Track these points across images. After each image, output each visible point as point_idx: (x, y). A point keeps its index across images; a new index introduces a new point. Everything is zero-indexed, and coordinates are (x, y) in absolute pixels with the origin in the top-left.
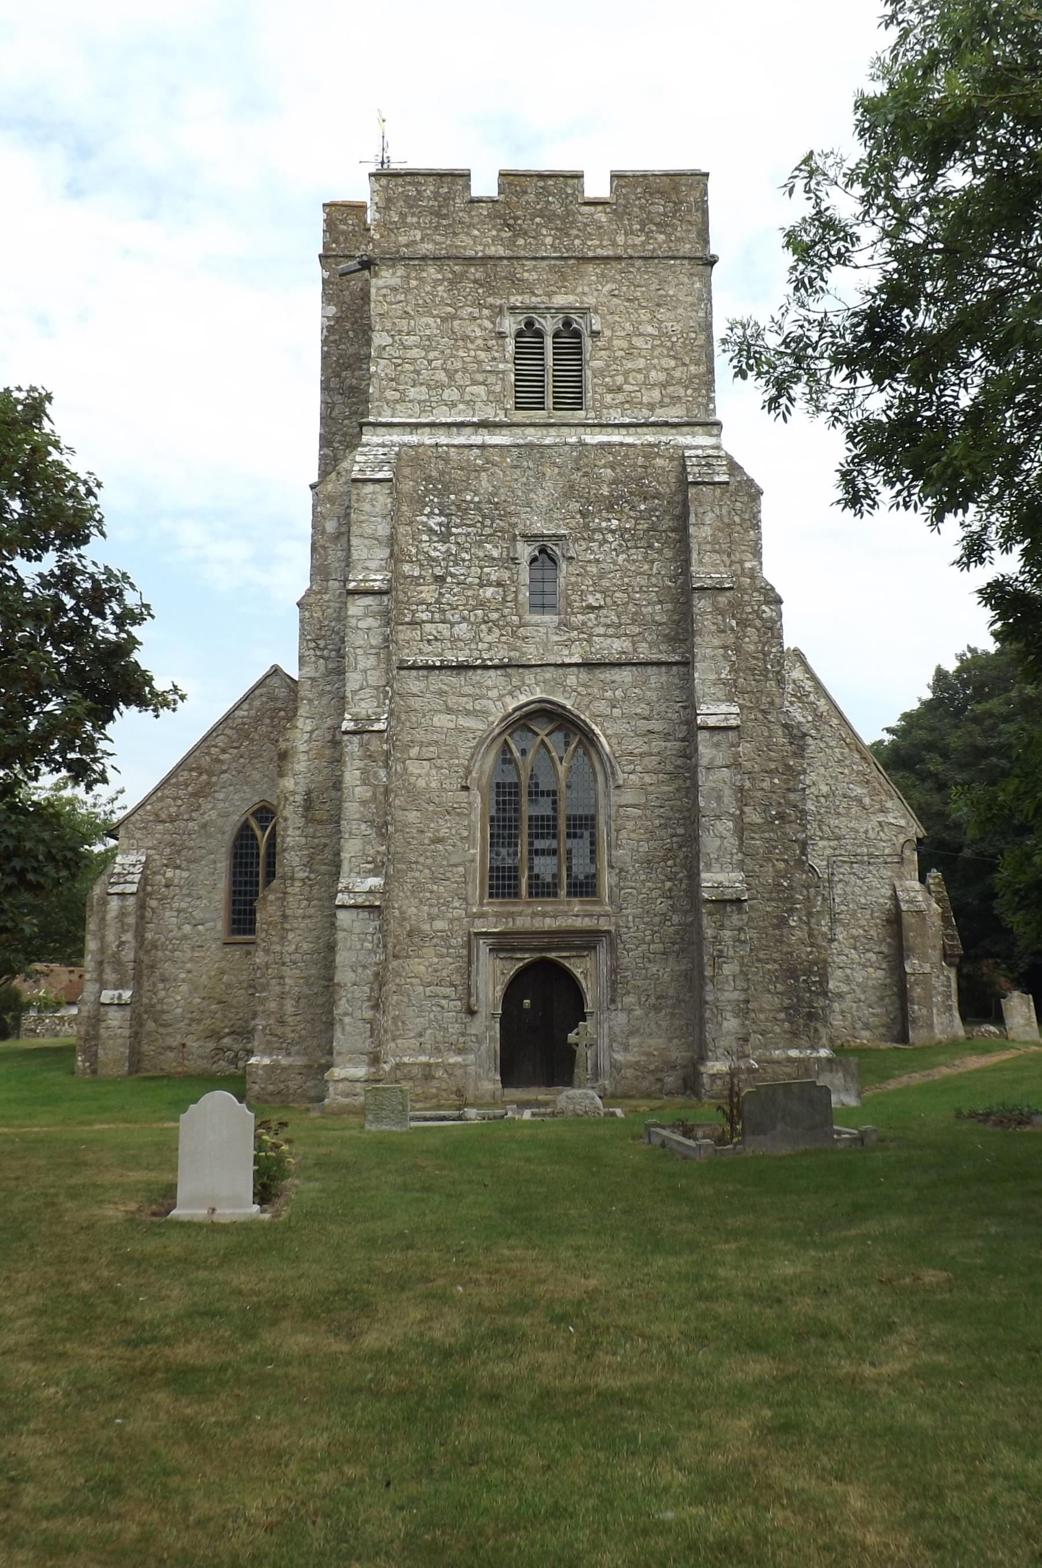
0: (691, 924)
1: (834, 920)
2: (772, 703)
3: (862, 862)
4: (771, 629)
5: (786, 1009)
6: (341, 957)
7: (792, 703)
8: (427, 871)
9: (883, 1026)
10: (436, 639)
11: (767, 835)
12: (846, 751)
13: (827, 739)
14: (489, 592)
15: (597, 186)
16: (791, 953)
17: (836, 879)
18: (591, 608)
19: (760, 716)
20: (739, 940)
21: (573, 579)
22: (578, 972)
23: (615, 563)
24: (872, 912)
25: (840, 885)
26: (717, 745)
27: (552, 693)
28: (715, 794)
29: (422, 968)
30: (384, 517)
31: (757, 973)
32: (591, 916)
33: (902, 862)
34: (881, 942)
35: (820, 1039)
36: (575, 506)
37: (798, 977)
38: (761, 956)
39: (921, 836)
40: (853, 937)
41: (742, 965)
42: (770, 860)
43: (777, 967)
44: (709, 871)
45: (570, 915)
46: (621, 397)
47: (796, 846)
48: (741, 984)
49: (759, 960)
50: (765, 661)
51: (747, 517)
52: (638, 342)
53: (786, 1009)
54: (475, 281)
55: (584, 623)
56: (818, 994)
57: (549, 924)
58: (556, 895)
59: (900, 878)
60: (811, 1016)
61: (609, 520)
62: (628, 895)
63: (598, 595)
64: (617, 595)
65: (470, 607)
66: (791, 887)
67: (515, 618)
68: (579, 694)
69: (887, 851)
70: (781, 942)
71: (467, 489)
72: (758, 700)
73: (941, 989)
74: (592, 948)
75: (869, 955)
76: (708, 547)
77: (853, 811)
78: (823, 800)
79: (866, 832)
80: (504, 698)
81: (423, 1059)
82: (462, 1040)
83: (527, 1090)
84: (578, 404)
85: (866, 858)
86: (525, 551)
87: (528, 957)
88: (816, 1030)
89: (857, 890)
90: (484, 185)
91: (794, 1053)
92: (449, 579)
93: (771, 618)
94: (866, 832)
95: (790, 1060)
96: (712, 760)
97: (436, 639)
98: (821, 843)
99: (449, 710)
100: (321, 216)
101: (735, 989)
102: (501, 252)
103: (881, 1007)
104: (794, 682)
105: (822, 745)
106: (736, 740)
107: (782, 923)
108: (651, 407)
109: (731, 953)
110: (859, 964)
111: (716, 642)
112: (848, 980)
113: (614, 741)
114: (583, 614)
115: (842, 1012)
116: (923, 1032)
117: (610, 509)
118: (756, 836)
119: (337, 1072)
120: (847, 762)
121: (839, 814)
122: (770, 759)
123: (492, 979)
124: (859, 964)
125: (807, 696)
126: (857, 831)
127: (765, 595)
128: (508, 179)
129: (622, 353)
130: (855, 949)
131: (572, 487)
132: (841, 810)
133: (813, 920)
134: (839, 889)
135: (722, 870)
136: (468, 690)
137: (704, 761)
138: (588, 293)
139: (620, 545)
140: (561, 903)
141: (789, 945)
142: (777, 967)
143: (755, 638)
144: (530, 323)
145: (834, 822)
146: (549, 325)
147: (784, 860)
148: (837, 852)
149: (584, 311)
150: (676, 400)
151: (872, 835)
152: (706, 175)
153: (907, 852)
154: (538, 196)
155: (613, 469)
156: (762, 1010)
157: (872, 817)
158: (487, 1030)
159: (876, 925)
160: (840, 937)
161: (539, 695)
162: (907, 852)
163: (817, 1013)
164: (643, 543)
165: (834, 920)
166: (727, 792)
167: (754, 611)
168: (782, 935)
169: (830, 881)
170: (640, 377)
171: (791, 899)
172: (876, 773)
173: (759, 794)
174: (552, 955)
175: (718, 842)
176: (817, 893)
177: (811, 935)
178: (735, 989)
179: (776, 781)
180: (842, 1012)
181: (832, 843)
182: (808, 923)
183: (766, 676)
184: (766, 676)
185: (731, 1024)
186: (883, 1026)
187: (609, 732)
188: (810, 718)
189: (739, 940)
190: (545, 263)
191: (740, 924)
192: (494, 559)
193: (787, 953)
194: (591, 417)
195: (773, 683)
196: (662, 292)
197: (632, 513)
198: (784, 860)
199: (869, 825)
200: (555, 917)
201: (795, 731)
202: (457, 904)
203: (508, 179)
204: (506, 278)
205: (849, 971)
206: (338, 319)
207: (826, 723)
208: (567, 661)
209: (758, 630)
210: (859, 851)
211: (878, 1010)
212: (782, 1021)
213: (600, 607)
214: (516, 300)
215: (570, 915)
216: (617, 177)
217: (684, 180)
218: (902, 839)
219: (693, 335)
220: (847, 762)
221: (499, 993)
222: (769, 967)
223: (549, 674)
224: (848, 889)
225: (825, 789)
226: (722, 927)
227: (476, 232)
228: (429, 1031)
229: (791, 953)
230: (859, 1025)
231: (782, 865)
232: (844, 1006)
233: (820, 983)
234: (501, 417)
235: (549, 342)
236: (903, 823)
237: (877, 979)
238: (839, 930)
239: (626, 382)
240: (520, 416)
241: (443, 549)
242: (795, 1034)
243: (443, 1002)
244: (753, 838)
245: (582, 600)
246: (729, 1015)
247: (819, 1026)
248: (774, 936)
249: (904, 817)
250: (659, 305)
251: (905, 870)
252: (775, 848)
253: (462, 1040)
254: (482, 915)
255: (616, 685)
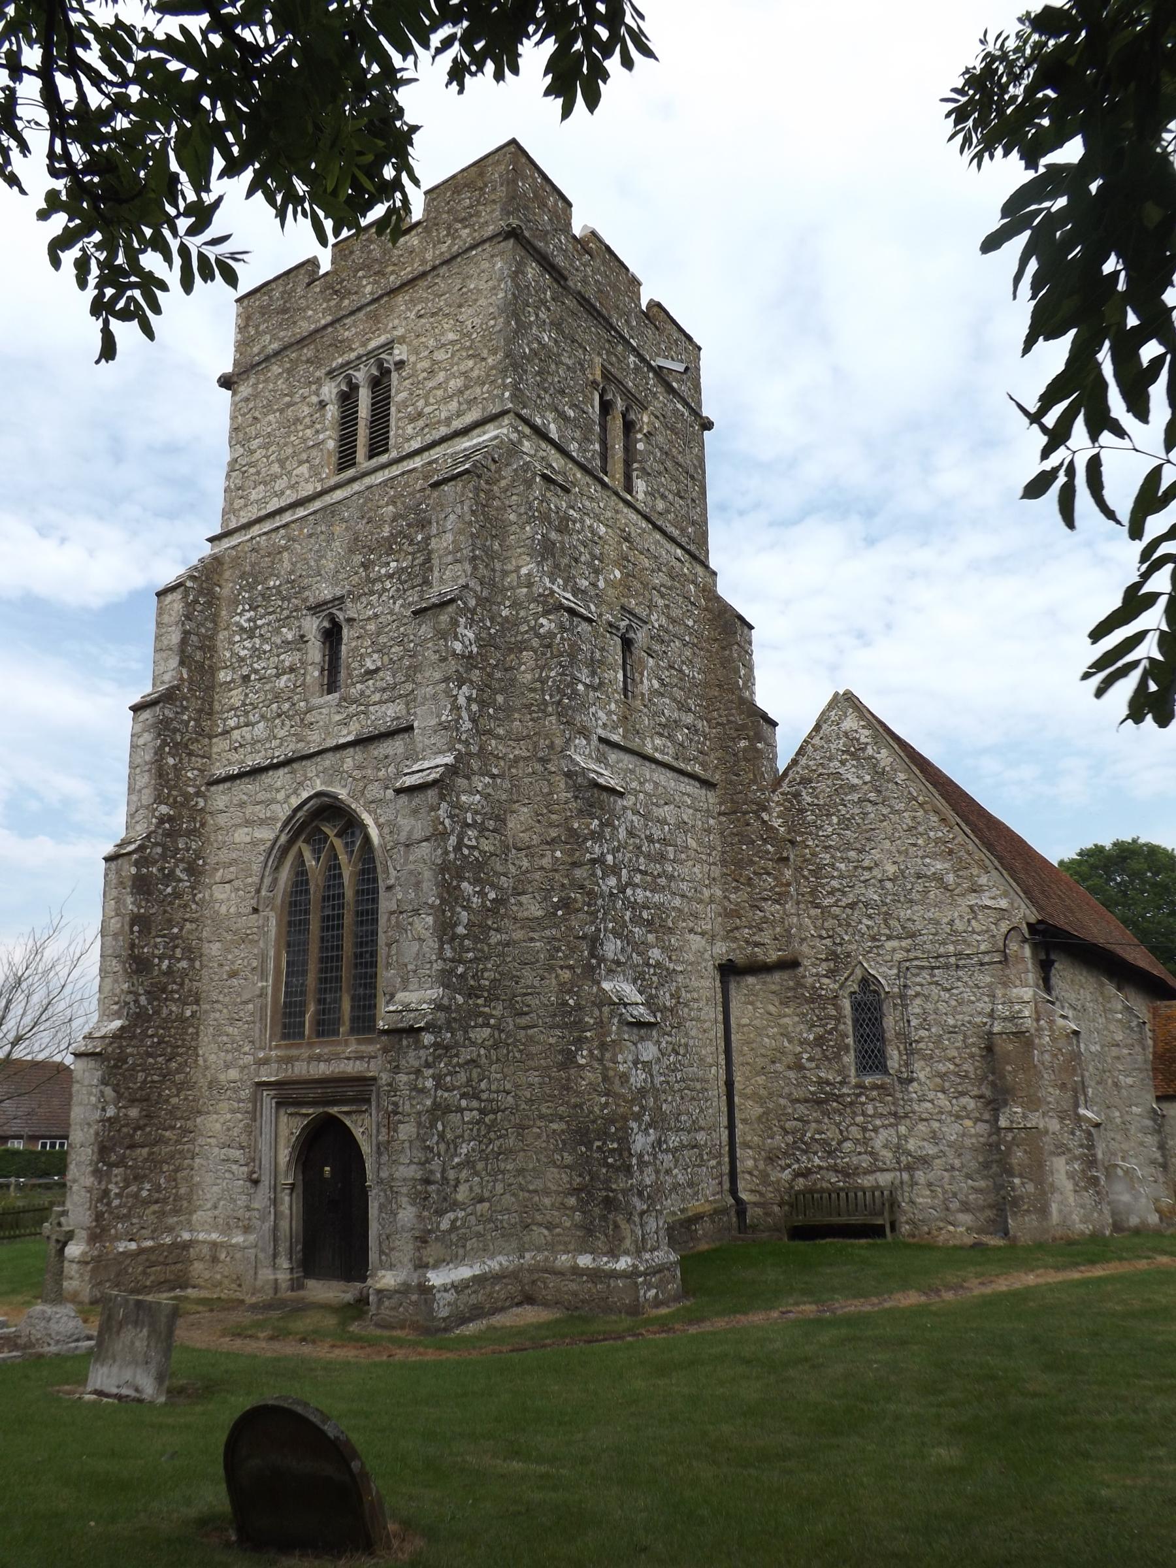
0: (644, 1067)
1: (910, 1050)
2: (551, 746)
3: (947, 967)
4: (549, 646)
5: (575, 1191)
7: (843, 763)
8: (225, 1011)
9: (991, 1207)
10: (241, 746)
11: (548, 933)
12: (920, 813)
13: (893, 802)
14: (282, 682)
16: (580, 1106)
17: (911, 992)
18: (371, 673)
19: (539, 767)
20: (415, 1088)
21: (354, 644)
22: (357, 1132)
23: (391, 613)
24: (965, 1036)
25: (918, 1001)
26: (415, 812)
27: (331, 783)
28: (413, 880)
29: (218, 1126)
30: (177, 624)
31: (539, 1136)
32: (361, 1058)
33: (1005, 961)
34: (982, 1079)
35: (622, 1240)
36: (358, 559)
37: (591, 1143)
38: (544, 1110)
39: (1032, 920)
40: (942, 1076)
41: (419, 1124)
42: (551, 969)
43: (564, 1126)
44: (405, 989)
46: (421, 423)
47: (584, 945)
48: (420, 1155)
49: (542, 1117)
50: (543, 690)
51: (522, 510)
52: (440, 355)
53: (575, 1191)
54: (308, 361)
55: (362, 693)
56: (618, 1170)
57: (322, 1069)
58: (336, 1033)
59: (1005, 985)
60: (609, 1203)
61: (388, 563)
63: (375, 656)
64: (393, 650)
65: (267, 703)
66: (579, 1007)
67: (302, 704)
68: (354, 779)
69: (983, 948)
70: (568, 1089)
71: (272, 575)
72: (535, 745)
73: (1078, 1151)
75: (964, 1100)
76: (450, 558)
77: (932, 895)
78: (889, 885)
79: (951, 923)
80: (286, 795)
81: (214, 1236)
82: (247, 1215)
83: (327, 1283)
85: (952, 960)
86: (312, 626)
88: (617, 1226)
89: (942, 1007)
91: (585, 1261)
92: (253, 677)
93: (549, 632)
94: (951, 923)
95: (576, 1271)
96: (410, 832)
97: (241, 746)
98: (889, 945)
99: (248, 823)
101: (411, 1162)
103: (984, 1178)
104: (846, 734)
105: (885, 811)
106: (435, 800)
107: (569, 1060)
109: (407, 1107)
110: (950, 1113)
111: (438, 676)
112: (934, 1138)
113: (386, 830)
114: (362, 682)
115: (930, 1185)
116: (1032, 1221)
117: (390, 552)
118: (536, 935)
120: (921, 829)
121: (911, 901)
122: (551, 825)
124: (950, 1113)
125: (864, 750)
126: (938, 923)
127: (544, 603)
129: (425, 374)
130: (944, 1092)
131: (356, 539)
132: (915, 896)
133: (608, 1055)
134: (915, 1007)
135: (420, 988)
136: (262, 796)
139: (398, 590)
140: (339, 1043)
141: (578, 1094)
142: (564, 1126)
143: (532, 663)
145: (905, 913)
147: (570, 967)
148: (912, 955)
150: (472, 402)
151: (959, 925)
153: (1013, 946)
155: (394, 503)
156: (547, 1192)
157: (959, 900)
159: (972, 1056)
160: (922, 1076)
161: (319, 787)
162: (1013, 946)
163: (615, 1198)
164: (419, 580)
165: (910, 1053)
166: (427, 874)
167: (532, 628)
168: (568, 1079)
169: (902, 996)
170: (440, 393)
171: (579, 1025)
172: (961, 838)
173: (538, 875)
174: (334, 1110)
175: (415, 946)
176: (612, 1014)
177: (606, 1078)
178: (411, 1162)
179: (558, 854)
180: (930, 1185)
181: (904, 944)
182: (601, 1060)
183: (544, 711)
184: (544, 711)
185: (407, 1214)
186: (991, 1207)
187: (382, 820)
188: (868, 778)
189: (415, 1088)
190: (361, 315)
191: (416, 1064)
192: (289, 643)
193: (575, 1106)
194: (394, 454)
195: (553, 718)
196: (464, 290)
197: (410, 549)
198: (570, 967)
199: (956, 913)
200: (328, 1061)
201: (580, 780)
202: (247, 1049)
203: (656, 305)
204: (330, 345)
205: (936, 1125)
207: (888, 781)
208: (342, 741)
209: (535, 652)
210: (942, 950)
211: (982, 1184)
212: (573, 1209)
213: (377, 670)
217: (490, 160)
218: (1004, 927)
219: (492, 322)
220: (921, 829)
222: (554, 1126)
223: (328, 761)
224: (929, 1006)
225: (891, 869)
226: (396, 1070)
227: (310, 313)
228: (222, 1203)
229: (580, 1106)
230: (954, 1205)
231: (566, 975)
232: (931, 1176)
233: (619, 1151)
236: (1003, 903)
237: (977, 1135)
238: (918, 1065)
239: (427, 404)
241: (250, 646)
242: (589, 1231)
243: (234, 1167)
244: (532, 940)
245: (362, 666)
246: (404, 1200)
247: (620, 1219)
248: (559, 1080)
249: (1005, 895)
250: (460, 306)
251: (1012, 972)
252: (558, 950)
253: (247, 1215)
254: (265, 1062)
255: (389, 760)
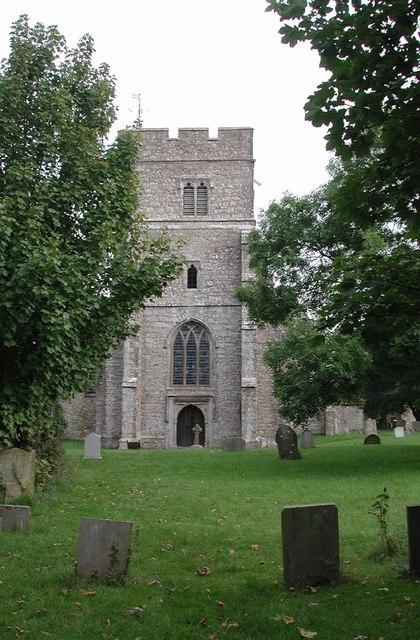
6: (124, 403)
15: (213, 134)
45: (199, 390)
46: (220, 211)
62: (220, 386)
74: (207, 402)
84: (206, 213)
87: (186, 404)
90: (174, 134)
99: (160, 321)
100: (213, 121)
102: (179, 158)
108: (231, 214)
119: (123, 440)
123: (173, 411)
128: (182, 132)
137: (243, 341)
138: (208, 173)
144: (189, 184)
146: (195, 185)
149: (208, 180)
152: (251, 131)
154: (192, 137)
158: (172, 428)
194: (209, 218)
203: (182, 132)
206: (107, 100)
214: (184, 176)
215: (199, 390)
216: (221, 131)
221: (176, 416)
234: (178, 218)
235: (196, 191)
240: (185, 218)
